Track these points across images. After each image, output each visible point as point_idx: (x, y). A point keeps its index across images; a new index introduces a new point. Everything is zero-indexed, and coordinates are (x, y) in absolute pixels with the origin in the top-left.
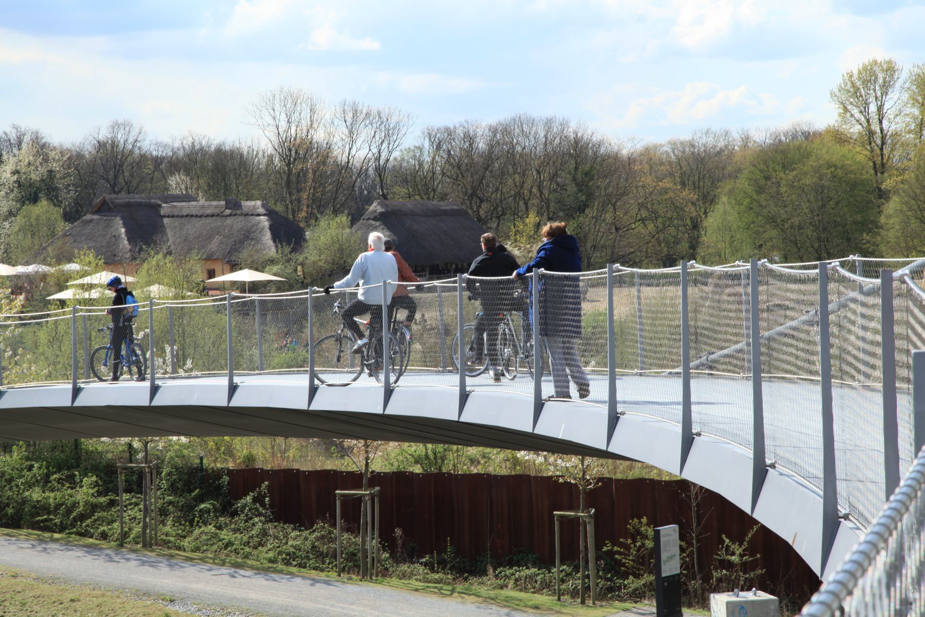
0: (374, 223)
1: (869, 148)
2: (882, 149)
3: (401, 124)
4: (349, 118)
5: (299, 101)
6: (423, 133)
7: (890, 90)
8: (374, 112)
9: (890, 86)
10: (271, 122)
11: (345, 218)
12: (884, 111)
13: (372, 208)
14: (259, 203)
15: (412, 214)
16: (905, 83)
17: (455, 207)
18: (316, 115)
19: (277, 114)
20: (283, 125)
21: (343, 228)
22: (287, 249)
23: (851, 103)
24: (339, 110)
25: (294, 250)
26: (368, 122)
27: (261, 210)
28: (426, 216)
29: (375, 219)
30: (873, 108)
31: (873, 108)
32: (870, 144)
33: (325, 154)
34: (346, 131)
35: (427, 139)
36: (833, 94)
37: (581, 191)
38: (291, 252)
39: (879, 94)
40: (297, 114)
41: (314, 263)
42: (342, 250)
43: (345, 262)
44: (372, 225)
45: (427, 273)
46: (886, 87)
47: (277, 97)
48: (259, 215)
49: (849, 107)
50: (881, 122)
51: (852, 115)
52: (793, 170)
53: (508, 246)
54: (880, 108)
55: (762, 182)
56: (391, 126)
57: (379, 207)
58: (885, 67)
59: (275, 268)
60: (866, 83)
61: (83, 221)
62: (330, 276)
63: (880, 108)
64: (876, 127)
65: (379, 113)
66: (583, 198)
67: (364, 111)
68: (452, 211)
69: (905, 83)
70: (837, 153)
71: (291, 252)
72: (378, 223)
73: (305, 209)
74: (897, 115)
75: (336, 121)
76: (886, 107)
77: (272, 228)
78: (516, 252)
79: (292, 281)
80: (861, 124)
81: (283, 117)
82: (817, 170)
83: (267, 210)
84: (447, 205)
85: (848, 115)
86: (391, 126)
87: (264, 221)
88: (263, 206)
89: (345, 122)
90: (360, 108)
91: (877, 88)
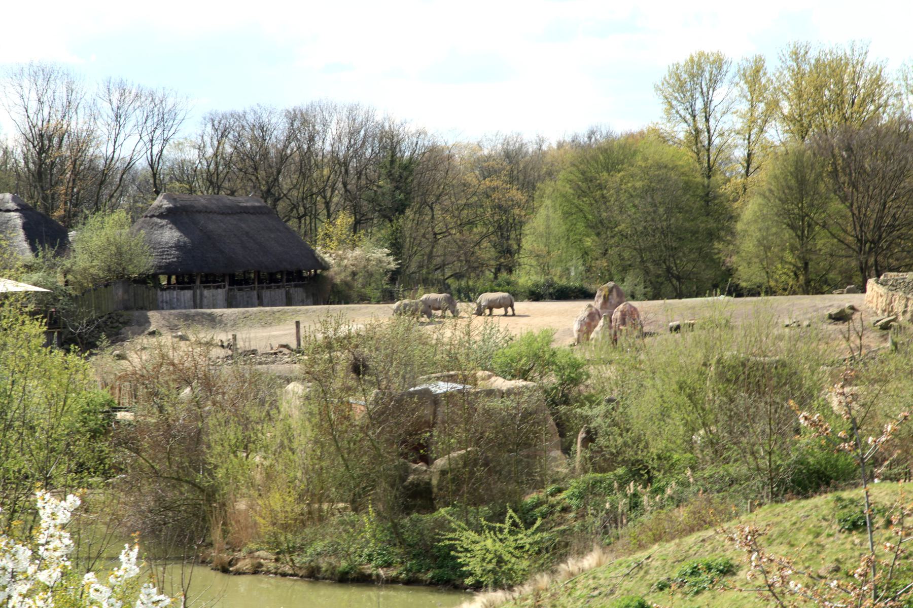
0: (159, 221)
1: (694, 148)
2: (708, 150)
3: (179, 107)
4: (115, 97)
5: (53, 78)
6: (205, 119)
7: (719, 84)
8: (146, 92)
9: (716, 82)
10: (19, 101)
11: (125, 214)
12: (712, 107)
13: (156, 203)
14: (8, 196)
15: (206, 211)
16: (734, 77)
17: (257, 204)
18: (74, 93)
19: (26, 91)
20: (33, 105)
21: (122, 226)
22: (50, 254)
23: (676, 98)
24: (103, 90)
25: (57, 254)
26: (138, 104)
27: (12, 205)
28: (223, 214)
29: (161, 216)
30: (699, 105)
31: (699, 105)
32: (697, 144)
33: (79, 147)
34: (112, 115)
35: (209, 126)
36: (657, 88)
37: (397, 188)
38: (54, 257)
39: (705, 90)
40: (50, 92)
41: (85, 269)
42: (121, 254)
43: (124, 269)
44: (156, 224)
45: (227, 284)
46: (713, 82)
47: (26, 71)
48: (8, 211)
49: (674, 103)
50: (707, 120)
51: (677, 112)
52: (619, 171)
53: (319, 249)
54: (707, 105)
55: (584, 186)
56: (166, 110)
57: (165, 202)
58: (712, 59)
59: (35, 276)
60: (692, 76)
61: (839, 499)
62: (106, 286)
63: (707, 105)
64: (701, 125)
65: (152, 94)
66: (402, 196)
67: (134, 92)
68: (254, 208)
69: (734, 77)
70: (667, 153)
71: (54, 257)
72: (164, 222)
73: (62, 206)
74: (724, 113)
75: (99, 101)
76: (714, 104)
77: (25, 227)
78: (327, 258)
79: (57, 293)
80: (686, 122)
81: (34, 97)
82: (645, 171)
83: (19, 205)
84: (247, 201)
85: (674, 111)
86: (166, 110)
87: (16, 219)
88: (14, 199)
89: (111, 103)
90: (128, 88)
91: (703, 83)
